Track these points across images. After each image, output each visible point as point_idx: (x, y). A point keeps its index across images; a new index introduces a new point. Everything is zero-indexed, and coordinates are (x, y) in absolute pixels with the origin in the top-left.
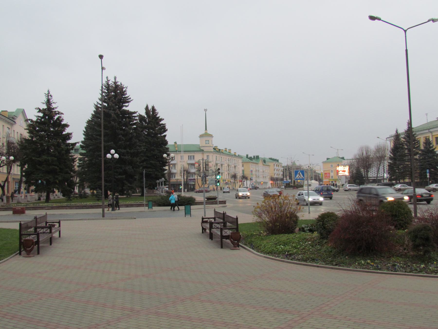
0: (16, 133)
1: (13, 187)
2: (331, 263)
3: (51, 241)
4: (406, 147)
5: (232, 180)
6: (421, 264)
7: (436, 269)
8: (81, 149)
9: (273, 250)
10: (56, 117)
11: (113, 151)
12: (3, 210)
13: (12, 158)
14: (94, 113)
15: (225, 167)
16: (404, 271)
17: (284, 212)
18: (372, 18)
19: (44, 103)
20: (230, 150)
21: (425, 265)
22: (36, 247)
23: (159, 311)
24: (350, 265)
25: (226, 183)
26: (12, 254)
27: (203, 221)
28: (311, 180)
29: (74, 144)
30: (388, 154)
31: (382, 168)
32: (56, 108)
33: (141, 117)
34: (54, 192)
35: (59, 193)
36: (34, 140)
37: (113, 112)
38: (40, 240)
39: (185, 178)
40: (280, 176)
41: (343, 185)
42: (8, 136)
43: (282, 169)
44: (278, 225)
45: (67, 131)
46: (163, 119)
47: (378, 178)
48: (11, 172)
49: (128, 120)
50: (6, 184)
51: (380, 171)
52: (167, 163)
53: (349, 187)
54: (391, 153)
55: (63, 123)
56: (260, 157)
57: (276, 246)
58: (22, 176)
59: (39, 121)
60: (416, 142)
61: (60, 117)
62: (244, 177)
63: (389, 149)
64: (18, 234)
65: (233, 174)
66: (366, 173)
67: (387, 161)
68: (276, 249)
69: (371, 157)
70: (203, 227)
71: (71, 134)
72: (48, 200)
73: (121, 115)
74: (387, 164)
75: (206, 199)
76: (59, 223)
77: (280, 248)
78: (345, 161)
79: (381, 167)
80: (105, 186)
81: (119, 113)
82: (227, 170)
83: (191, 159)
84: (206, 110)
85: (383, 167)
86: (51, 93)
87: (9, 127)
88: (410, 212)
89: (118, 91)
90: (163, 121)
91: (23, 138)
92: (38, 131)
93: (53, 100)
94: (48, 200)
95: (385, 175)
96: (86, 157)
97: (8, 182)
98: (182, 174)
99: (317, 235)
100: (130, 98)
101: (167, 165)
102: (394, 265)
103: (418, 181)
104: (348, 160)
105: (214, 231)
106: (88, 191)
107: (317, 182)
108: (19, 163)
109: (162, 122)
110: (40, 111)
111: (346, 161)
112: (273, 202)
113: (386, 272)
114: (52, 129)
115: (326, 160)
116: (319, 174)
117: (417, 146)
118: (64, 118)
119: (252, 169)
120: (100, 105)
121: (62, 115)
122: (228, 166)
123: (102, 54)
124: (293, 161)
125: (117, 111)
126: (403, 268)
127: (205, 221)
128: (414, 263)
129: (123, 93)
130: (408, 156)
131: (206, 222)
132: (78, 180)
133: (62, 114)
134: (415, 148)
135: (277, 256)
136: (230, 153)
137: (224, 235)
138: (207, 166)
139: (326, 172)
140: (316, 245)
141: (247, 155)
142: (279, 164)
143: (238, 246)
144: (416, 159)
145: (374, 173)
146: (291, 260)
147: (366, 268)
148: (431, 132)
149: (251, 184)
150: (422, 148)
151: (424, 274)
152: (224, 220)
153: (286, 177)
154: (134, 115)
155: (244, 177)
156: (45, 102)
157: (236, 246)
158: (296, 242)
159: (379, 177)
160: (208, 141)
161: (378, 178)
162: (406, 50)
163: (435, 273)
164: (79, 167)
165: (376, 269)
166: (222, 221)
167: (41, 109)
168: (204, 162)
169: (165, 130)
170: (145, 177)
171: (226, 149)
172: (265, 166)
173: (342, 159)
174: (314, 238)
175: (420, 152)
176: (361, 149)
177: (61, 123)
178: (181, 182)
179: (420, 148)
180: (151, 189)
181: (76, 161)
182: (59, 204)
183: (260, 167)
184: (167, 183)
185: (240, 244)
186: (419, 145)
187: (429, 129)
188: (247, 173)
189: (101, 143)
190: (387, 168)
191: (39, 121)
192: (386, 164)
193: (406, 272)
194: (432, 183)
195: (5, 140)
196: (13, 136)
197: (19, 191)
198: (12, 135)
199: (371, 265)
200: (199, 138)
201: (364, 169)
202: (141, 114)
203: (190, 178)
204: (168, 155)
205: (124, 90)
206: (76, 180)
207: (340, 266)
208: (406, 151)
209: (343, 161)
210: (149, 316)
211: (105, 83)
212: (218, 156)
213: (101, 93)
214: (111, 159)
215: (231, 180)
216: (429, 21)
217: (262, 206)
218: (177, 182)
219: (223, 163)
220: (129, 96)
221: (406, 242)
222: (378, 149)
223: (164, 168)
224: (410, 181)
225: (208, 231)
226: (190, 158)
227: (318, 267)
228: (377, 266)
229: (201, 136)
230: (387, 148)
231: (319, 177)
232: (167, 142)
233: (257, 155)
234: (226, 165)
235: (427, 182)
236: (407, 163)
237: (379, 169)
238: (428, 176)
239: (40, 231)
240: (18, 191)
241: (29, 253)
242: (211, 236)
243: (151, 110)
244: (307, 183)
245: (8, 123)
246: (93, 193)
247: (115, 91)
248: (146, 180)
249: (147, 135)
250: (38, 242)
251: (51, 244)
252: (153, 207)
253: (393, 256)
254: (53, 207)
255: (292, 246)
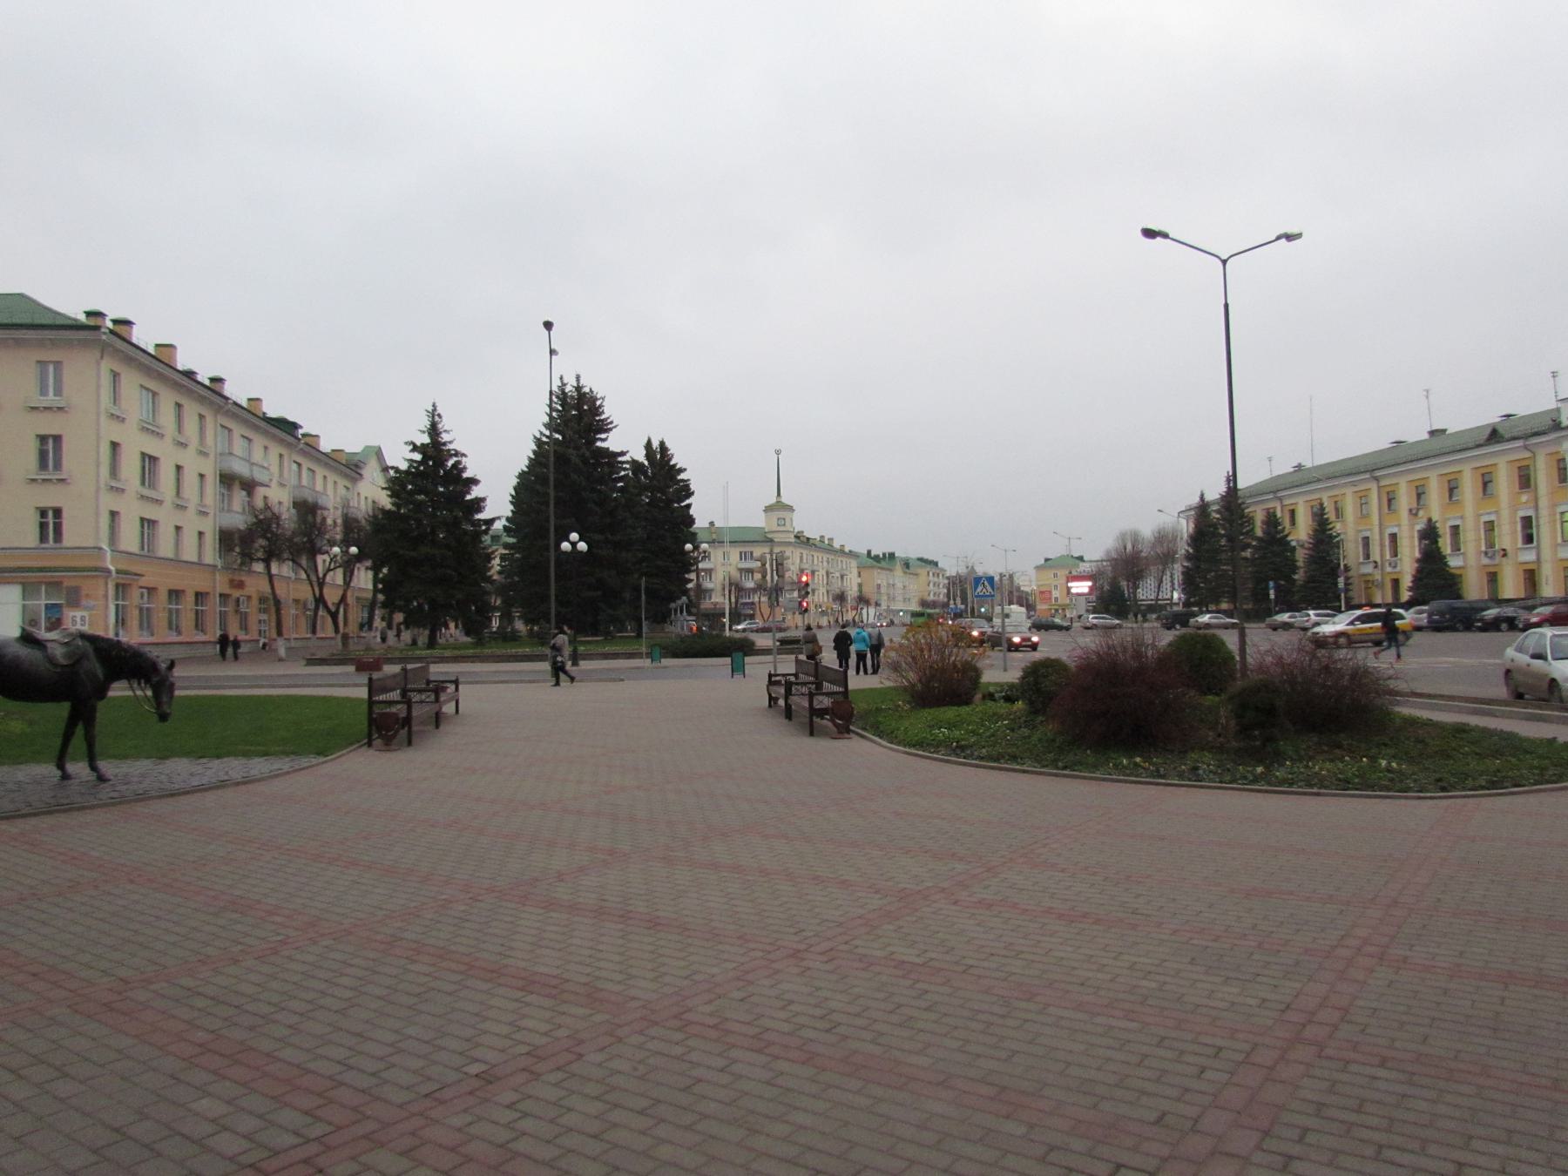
0: (363, 498)
1: (357, 617)
2: (1055, 765)
3: (438, 719)
4: (1223, 532)
5: (836, 607)
6: (1255, 766)
7: (1290, 776)
8: (505, 534)
9: (924, 737)
10: (450, 463)
11: (574, 536)
12: (335, 664)
13: (354, 550)
14: (533, 457)
15: (821, 594)
16: (1217, 780)
17: (949, 660)
18: (1149, 233)
19: (424, 432)
20: (831, 540)
21: (1265, 768)
22: (404, 732)
23: (671, 853)
24: (1095, 767)
25: (823, 613)
26: (351, 744)
27: (772, 681)
28: (1009, 605)
29: (490, 522)
30: (1183, 548)
31: (1169, 579)
32: (450, 442)
33: (635, 464)
34: (447, 627)
35: (458, 631)
36: (402, 511)
37: (575, 452)
38: (414, 713)
39: (733, 600)
40: (941, 596)
41: (1080, 617)
42: (346, 505)
43: (946, 581)
44: (936, 687)
45: (476, 492)
46: (685, 470)
47: (1160, 602)
48: (352, 585)
49: (606, 469)
50: (342, 610)
51: (1165, 587)
52: (692, 565)
53: (1095, 621)
54: (1189, 545)
55: (465, 475)
56: (896, 555)
57: (930, 731)
58: (376, 590)
59: (413, 470)
60: (1245, 520)
61: (458, 462)
62: (863, 600)
63: (1185, 536)
64: (365, 707)
65: (838, 591)
66: (1131, 590)
67: (1179, 565)
68: (931, 736)
69: (1143, 554)
70: (770, 695)
71: (483, 500)
72: (432, 643)
73: (592, 458)
74: (1180, 569)
75: (778, 643)
76: (456, 683)
77: (941, 735)
78: (1084, 564)
79: (1166, 579)
80: (558, 614)
81: (587, 454)
82: (825, 582)
83: (745, 559)
84: (778, 452)
85: (1171, 577)
86: (439, 410)
87: (349, 485)
88: (1233, 658)
89: (585, 407)
90: (686, 473)
91: (379, 509)
92: (412, 493)
93: (444, 424)
94: (432, 643)
95: (1176, 595)
96: (516, 553)
97: (346, 605)
98: (727, 592)
99: (1024, 706)
100: (612, 422)
101: (693, 571)
102: (1196, 769)
103: (1250, 606)
104: (1091, 561)
105: (794, 699)
106: (520, 626)
107: (1023, 610)
108: (369, 563)
109: (682, 476)
110: (415, 448)
111: (1088, 565)
112: (924, 637)
113: (1176, 782)
114: (441, 489)
115: (1043, 562)
116: (1027, 593)
117: (1248, 528)
118: (467, 465)
119: (879, 582)
120: (547, 437)
121: (464, 459)
122: (827, 573)
123: (550, 320)
124: (970, 565)
125: (584, 450)
126: (1215, 773)
127: (776, 681)
128: (1240, 765)
129: (596, 410)
130: (1225, 551)
131: (778, 683)
132: (499, 602)
133: (464, 455)
134: (1242, 534)
135: (932, 750)
136: (832, 546)
137: (818, 707)
138: (780, 567)
139: (1043, 589)
140: (1020, 727)
141: (869, 552)
142: (938, 571)
143: (849, 731)
144: (1246, 559)
145: (1149, 592)
146: (965, 758)
147: (1131, 774)
148: (1280, 499)
149: (878, 614)
150: (1259, 532)
151: (1263, 786)
152: (816, 676)
153: (954, 600)
154: (620, 459)
155: (863, 600)
156: (425, 429)
157: (844, 731)
158: (975, 721)
159: (1160, 600)
160: (784, 519)
161: (1160, 602)
162: (1226, 306)
163: (1289, 783)
164: (500, 573)
165: (1154, 777)
166: (812, 679)
167: (418, 444)
168: (774, 558)
169: (689, 494)
170: (645, 594)
171: (822, 537)
172: (908, 576)
173: (1077, 561)
174: (1016, 713)
175: (1254, 543)
176: (1123, 537)
177: (462, 476)
178: (724, 608)
179: (1254, 533)
180: (659, 623)
181: (494, 558)
182: (457, 653)
183: (899, 577)
184: (694, 610)
185: (852, 728)
186: (1251, 526)
187: (1275, 492)
188: (869, 591)
189: (547, 520)
190: (1181, 578)
191: (413, 470)
192: (1178, 569)
193: (1221, 782)
194: (1282, 611)
195: (339, 513)
196: (356, 505)
197: (368, 624)
198: (354, 503)
199: (1144, 768)
200: (763, 513)
201: (1128, 581)
202: (636, 458)
203: (744, 601)
204: (696, 548)
205: (598, 403)
206: (495, 602)
207: (1074, 770)
208: (1223, 542)
209: (1081, 564)
210: (650, 863)
211: (557, 390)
212: (805, 552)
213: (548, 412)
214: (571, 552)
215: (834, 606)
216: (1278, 238)
217: (900, 646)
218: (715, 608)
219: (815, 568)
220: (608, 418)
221: (1223, 721)
222: (1162, 538)
223: (686, 576)
224: (1232, 607)
225: (781, 702)
226: (744, 556)
227: (1024, 772)
228: (1158, 771)
229: (768, 509)
230: (1179, 534)
231: (1027, 600)
232: (694, 519)
233: (891, 551)
234: (821, 573)
235: (1270, 609)
236: (1225, 567)
237: (1161, 581)
238: (1272, 596)
239: (416, 697)
240: (366, 626)
241: (389, 743)
242: (789, 713)
243: (659, 450)
244: (1000, 611)
245: (346, 476)
246: (531, 630)
247: (578, 407)
248: (648, 603)
249: (648, 504)
250: (407, 721)
251: (437, 727)
252: (663, 660)
253: (1193, 749)
254: (444, 657)
255: (967, 730)
